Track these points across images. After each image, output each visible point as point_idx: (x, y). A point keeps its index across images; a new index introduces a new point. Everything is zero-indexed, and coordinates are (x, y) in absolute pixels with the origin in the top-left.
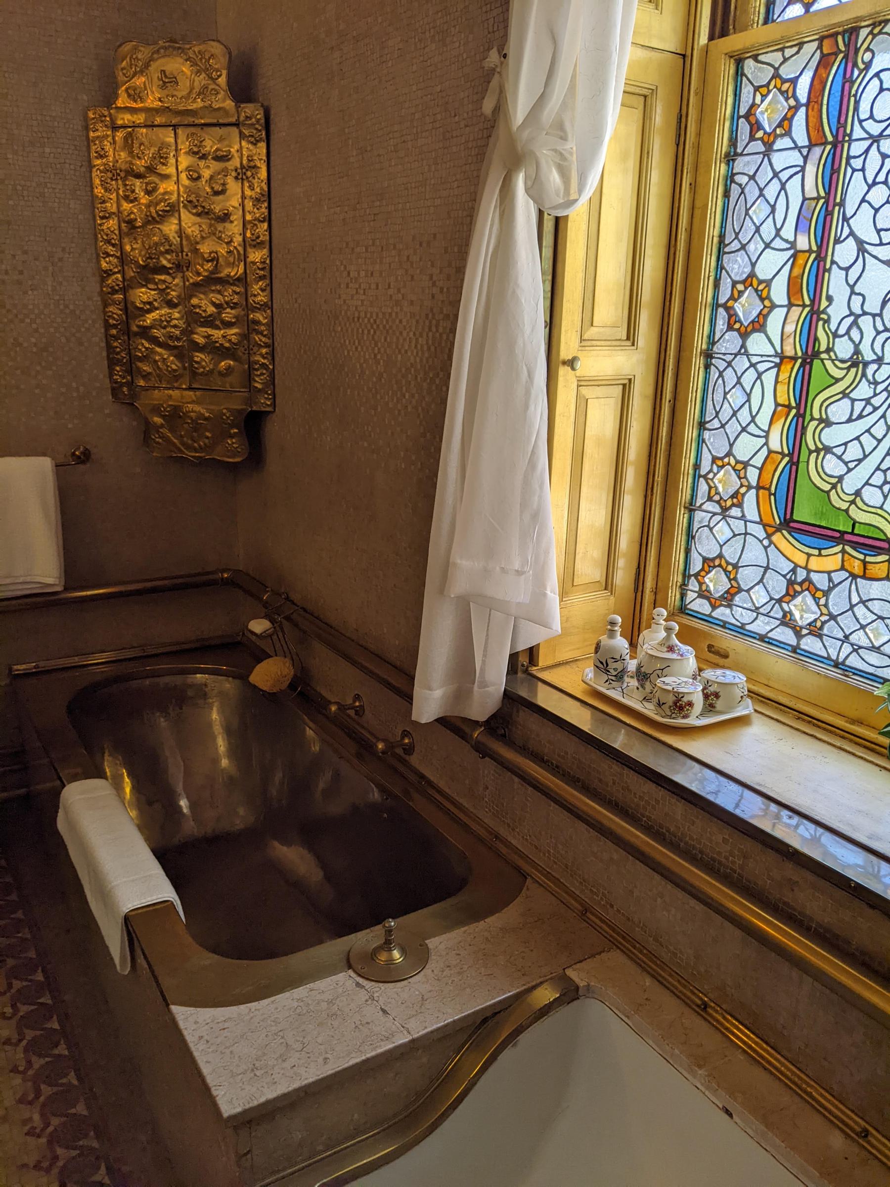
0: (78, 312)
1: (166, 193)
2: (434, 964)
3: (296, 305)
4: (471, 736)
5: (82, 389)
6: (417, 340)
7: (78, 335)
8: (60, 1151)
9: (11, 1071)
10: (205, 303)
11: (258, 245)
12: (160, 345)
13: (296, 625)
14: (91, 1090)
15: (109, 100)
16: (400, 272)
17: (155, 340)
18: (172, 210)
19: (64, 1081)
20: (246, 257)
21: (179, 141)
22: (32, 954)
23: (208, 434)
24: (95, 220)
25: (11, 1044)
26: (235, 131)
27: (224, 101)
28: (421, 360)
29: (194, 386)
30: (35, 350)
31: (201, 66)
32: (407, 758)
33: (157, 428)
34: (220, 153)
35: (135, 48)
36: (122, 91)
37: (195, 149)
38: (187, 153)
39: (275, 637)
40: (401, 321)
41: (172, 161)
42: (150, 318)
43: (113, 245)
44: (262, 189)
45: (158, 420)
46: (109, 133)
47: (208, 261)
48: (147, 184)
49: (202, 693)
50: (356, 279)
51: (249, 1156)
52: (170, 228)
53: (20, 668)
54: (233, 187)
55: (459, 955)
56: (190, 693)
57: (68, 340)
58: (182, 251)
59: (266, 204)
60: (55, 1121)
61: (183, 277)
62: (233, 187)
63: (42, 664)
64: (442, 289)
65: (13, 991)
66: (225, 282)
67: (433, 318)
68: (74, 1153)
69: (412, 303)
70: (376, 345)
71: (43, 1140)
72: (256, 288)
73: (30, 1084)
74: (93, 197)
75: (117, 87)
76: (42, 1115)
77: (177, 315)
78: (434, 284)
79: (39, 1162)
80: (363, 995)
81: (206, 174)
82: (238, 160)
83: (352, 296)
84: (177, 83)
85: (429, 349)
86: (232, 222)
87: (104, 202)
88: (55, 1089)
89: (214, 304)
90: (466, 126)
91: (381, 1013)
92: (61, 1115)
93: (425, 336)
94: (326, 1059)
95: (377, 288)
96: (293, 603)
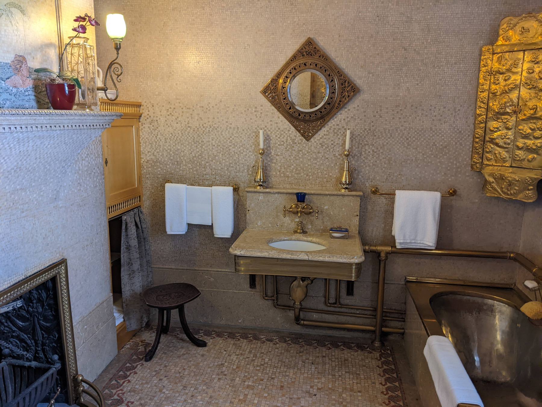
5: (458, 164)
10: (526, 128)
17: (497, 145)
18: (517, 87)
23: (517, 188)
24: (477, 93)
30: (441, 147)
33: (490, 183)
36: (500, 38)
37: (533, 60)
41: (520, 65)
42: (496, 135)
45: (491, 179)
46: (491, 56)
52: (514, 96)
53: (411, 278)
57: (456, 143)
58: (518, 105)
87: (483, 85)
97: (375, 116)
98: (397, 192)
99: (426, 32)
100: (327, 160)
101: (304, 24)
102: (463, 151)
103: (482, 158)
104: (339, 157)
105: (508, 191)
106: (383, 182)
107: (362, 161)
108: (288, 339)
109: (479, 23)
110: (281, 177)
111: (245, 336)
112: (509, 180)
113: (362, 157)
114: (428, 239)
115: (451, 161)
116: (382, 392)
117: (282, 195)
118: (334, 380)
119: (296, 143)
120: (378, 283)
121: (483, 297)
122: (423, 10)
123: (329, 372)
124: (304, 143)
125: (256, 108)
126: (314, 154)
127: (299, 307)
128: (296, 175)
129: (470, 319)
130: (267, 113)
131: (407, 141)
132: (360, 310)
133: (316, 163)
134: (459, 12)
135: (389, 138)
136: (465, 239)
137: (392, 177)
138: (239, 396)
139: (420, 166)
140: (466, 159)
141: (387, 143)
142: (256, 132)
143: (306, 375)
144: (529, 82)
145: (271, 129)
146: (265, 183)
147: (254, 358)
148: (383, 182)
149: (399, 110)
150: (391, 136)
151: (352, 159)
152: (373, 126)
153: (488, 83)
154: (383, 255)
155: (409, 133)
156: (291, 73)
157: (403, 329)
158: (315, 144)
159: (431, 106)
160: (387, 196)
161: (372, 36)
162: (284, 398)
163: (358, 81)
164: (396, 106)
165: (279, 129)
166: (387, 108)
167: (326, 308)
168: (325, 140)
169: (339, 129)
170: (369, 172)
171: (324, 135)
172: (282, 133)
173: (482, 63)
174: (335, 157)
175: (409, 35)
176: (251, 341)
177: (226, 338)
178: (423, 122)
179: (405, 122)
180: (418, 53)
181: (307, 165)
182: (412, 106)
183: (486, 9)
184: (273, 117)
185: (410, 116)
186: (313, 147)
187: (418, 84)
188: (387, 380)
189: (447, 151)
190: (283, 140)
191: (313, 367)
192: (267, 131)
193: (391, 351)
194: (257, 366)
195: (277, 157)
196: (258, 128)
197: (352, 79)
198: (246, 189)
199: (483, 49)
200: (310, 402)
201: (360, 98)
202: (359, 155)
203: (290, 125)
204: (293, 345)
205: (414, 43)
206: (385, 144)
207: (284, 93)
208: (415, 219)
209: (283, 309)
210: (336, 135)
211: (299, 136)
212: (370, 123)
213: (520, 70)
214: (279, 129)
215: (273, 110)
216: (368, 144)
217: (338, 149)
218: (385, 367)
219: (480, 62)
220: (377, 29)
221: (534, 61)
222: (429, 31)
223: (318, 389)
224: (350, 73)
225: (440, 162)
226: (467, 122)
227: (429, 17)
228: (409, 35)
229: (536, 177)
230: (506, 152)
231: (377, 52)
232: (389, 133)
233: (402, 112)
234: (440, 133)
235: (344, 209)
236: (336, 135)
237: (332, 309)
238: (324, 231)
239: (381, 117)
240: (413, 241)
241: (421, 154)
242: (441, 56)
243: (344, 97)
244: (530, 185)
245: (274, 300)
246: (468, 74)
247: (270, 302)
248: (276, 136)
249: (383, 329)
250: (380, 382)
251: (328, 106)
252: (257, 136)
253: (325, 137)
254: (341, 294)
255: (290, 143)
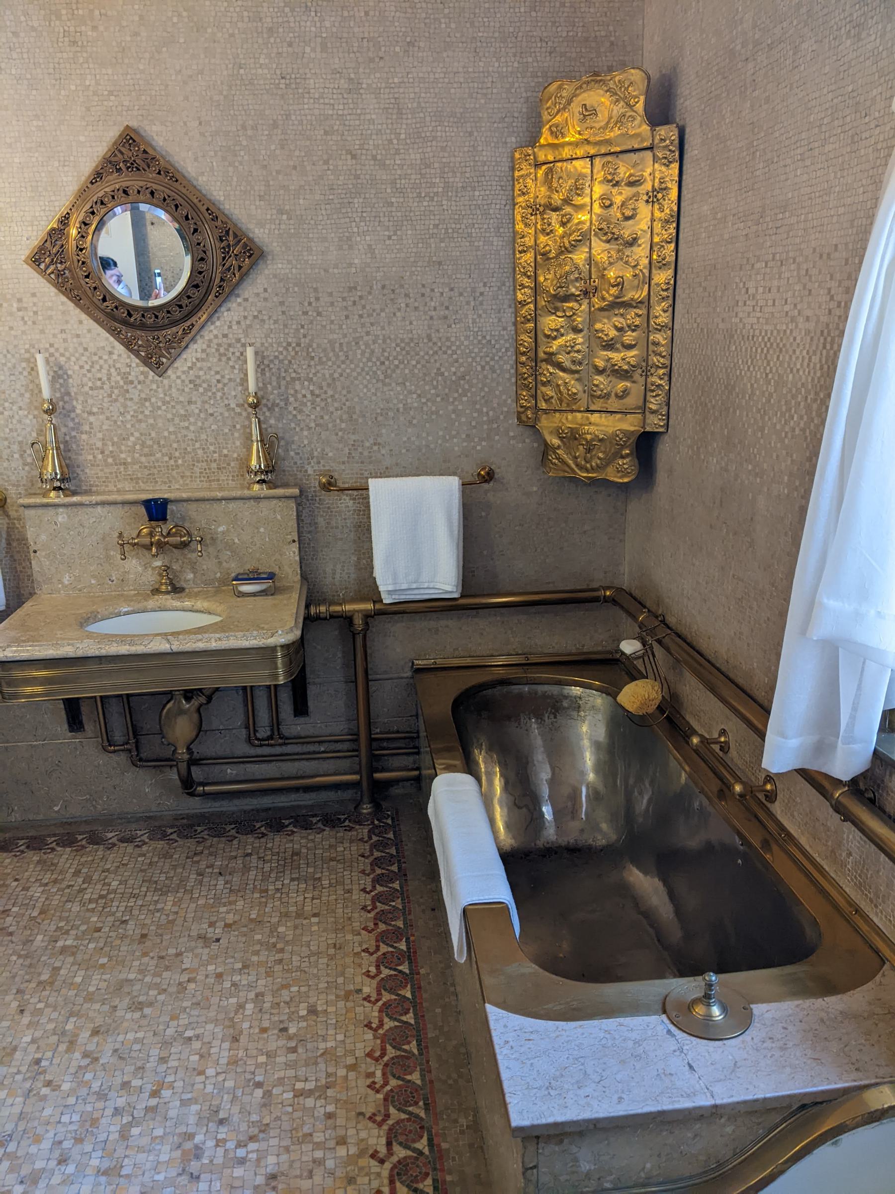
0: (493, 342)
1: (579, 223)
2: (755, 1032)
3: (695, 325)
4: (832, 795)
5: (491, 413)
6: (810, 358)
7: (492, 363)
8: (392, 1110)
9: (366, 1026)
10: (607, 327)
11: (663, 266)
12: (564, 370)
13: (668, 650)
14: (428, 1062)
15: (533, 141)
16: (797, 288)
17: (560, 366)
18: (585, 238)
19: (406, 1047)
20: (650, 279)
21: (595, 171)
22: (400, 924)
23: (601, 455)
24: (514, 254)
25: (369, 1001)
26: (649, 154)
27: (640, 127)
28: (813, 379)
29: (592, 408)
30: (454, 378)
31: (619, 95)
32: (769, 805)
33: (554, 449)
34: (632, 179)
35: (560, 88)
36: (545, 130)
37: (610, 177)
38: (600, 182)
39: (646, 658)
40: (795, 339)
41: (588, 191)
42: (555, 345)
43: (529, 277)
44: (671, 210)
45: (556, 442)
46: (532, 170)
47: (613, 286)
48: (563, 216)
49: (576, 705)
50: (754, 296)
51: (535, 1171)
52: (580, 257)
53: (420, 663)
54: (644, 211)
55: (785, 1028)
56: (565, 704)
57: (483, 368)
58: (590, 278)
59: (674, 225)
60: (393, 1082)
61: (589, 303)
62: (644, 211)
63: (438, 661)
64: (839, 303)
65: (379, 953)
66: (627, 305)
67: (829, 334)
68: (404, 1116)
69: (808, 319)
70: (768, 364)
71: (380, 1096)
72: (657, 310)
73: (379, 1041)
74: (515, 233)
75: (541, 128)
76: (384, 1074)
77: (580, 340)
78: (832, 298)
79: (374, 1115)
80: (672, 1045)
81: (618, 200)
82: (651, 184)
83: (749, 313)
84: (596, 115)
85: (821, 368)
86: (639, 246)
87: (523, 237)
88: (398, 1053)
89: (616, 328)
90: (877, 126)
91: (687, 1067)
92: (399, 1078)
93: (818, 353)
94: (620, 1098)
95: (774, 305)
96: (669, 627)
97: (305, 313)
98: (373, 483)
99: (394, 117)
100: (211, 419)
101: (111, 93)
102: (498, 383)
103: (535, 397)
104: (238, 410)
105: (587, 462)
106: (344, 463)
107: (290, 417)
108: (170, 831)
109: (504, 95)
110: (107, 465)
111: (68, 841)
112: (586, 439)
113: (291, 408)
114: (442, 577)
115: (478, 406)
116: (364, 908)
117: (112, 508)
118: (264, 900)
119: (132, 382)
120: (355, 682)
121: (560, 683)
122: (381, 64)
123: (255, 887)
124: (152, 381)
125: (20, 300)
126: (178, 407)
127: (186, 757)
128: (143, 459)
129: (534, 734)
130: (49, 313)
131: (383, 368)
132: (326, 745)
133: (187, 428)
134: (461, 70)
135: (343, 362)
136: (521, 567)
137: (360, 449)
138: (40, 974)
139: (415, 422)
140: (505, 401)
141: (341, 375)
142: (28, 361)
143: (201, 902)
144: (605, 227)
145: (66, 349)
146: (67, 482)
147: (85, 885)
148: (344, 463)
149: (357, 299)
150: (347, 357)
151: (268, 414)
152: (305, 336)
153: (532, 231)
154: (358, 621)
155: (384, 350)
156: (93, 213)
157: (418, 769)
158: (179, 381)
159: (423, 286)
160: (355, 493)
161: (275, 125)
162: (146, 960)
163: (257, 231)
164: (351, 289)
165: (86, 349)
166: (331, 294)
167: (253, 751)
168: (201, 373)
169: (230, 345)
170: (310, 443)
171: (197, 359)
172: (96, 358)
173: (517, 187)
174: (228, 410)
175: (357, 122)
176: (83, 847)
177: (22, 852)
178: (411, 323)
179: (372, 324)
180: (383, 165)
181: (166, 434)
182: (383, 287)
183: (516, 65)
184: (67, 322)
185: (382, 310)
186: (174, 390)
187: (390, 238)
188: (377, 880)
189: (467, 387)
190: (99, 375)
191: (221, 881)
192: (57, 355)
193: (393, 819)
194: (90, 901)
195: (92, 419)
196: (32, 351)
197: (244, 228)
198: (21, 501)
199: (517, 155)
200: (204, 957)
201: (266, 272)
202: (282, 404)
203: (112, 339)
204: (181, 842)
205: (371, 142)
206: (336, 375)
207: (83, 263)
208: (414, 537)
209: (155, 767)
210: (224, 359)
211: (137, 366)
212: (297, 330)
213: (588, 200)
214: (86, 349)
215: (63, 303)
216: (299, 379)
217: (233, 393)
218: (377, 854)
219: (514, 185)
220: (286, 107)
221: (611, 181)
222: (400, 113)
223: (227, 926)
224: (236, 212)
225: (454, 411)
226: (500, 320)
227: (396, 80)
228: (357, 122)
229: (632, 429)
230: (577, 380)
231: (291, 163)
232: (342, 350)
233: (363, 302)
234: (449, 347)
235: (262, 530)
236: (224, 359)
237: (266, 750)
238: (223, 582)
239: (319, 314)
240: (414, 586)
241: (415, 396)
242: (432, 171)
243: (229, 269)
244: (623, 447)
245: (130, 751)
246: (491, 211)
247: (122, 758)
248: (81, 367)
249: (377, 775)
250: (362, 887)
251: (195, 290)
252: (34, 369)
253: (199, 365)
254: (283, 715)
255: (117, 382)
